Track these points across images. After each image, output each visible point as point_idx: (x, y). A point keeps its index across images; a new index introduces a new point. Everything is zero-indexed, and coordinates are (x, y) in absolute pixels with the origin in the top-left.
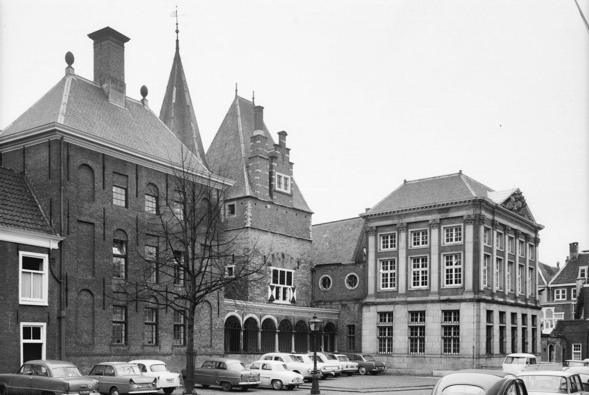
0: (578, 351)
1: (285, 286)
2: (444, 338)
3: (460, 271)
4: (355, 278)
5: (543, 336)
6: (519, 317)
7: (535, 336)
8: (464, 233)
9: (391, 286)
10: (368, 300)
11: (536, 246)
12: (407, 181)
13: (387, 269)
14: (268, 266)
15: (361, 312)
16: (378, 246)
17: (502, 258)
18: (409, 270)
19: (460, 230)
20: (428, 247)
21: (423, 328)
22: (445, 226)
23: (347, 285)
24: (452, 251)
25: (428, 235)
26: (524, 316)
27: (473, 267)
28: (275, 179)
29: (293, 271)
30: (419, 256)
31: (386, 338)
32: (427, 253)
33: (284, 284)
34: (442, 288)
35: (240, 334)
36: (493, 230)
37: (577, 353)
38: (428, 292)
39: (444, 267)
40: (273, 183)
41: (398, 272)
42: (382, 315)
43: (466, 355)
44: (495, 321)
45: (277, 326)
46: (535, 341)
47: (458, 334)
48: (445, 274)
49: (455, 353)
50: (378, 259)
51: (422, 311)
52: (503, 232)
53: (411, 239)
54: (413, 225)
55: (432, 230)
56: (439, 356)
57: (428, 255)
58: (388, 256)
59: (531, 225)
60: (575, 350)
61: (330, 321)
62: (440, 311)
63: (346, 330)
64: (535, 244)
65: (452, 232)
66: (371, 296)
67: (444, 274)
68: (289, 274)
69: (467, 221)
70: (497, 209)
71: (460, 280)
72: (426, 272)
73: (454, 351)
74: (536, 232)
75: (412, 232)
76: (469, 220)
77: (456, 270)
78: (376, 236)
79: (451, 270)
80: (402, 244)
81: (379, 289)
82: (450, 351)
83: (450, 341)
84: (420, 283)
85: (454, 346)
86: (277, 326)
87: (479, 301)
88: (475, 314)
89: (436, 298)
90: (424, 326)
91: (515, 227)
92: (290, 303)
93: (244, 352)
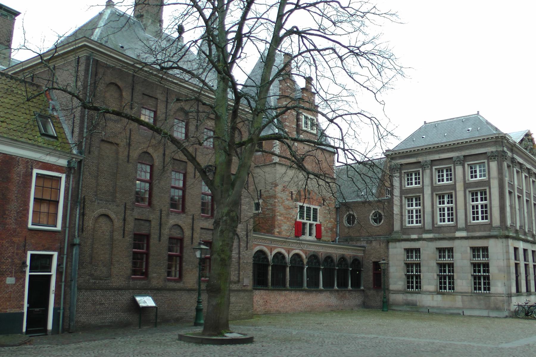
1: (312, 222)
2: (407, 275)
3: (452, 210)
6: (521, 252)
8: (455, 172)
9: (417, 223)
10: (394, 236)
13: (412, 206)
14: (295, 201)
15: (388, 249)
16: (434, 179)
18: (434, 206)
19: (451, 171)
21: (451, 265)
23: (372, 222)
24: (477, 187)
28: (302, 119)
29: (318, 208)
30: (444, 192)
32: (452, 189)
33: (310, 220)
35: (268, 269)
36: (513, 167)
38: (423, 230)
39: (436, 206)
40: (301, 123)
42: (409, 251)
43: (496, 294)
44: (530, 260)
45: (305, 261)
46: (519, 278)
47: (488, 271)
51: (450, 248)
52: (520, 171)
53: (435, 176)
54: (438, 162)
55: (456, 167)
56: (470, 294)
57: (453, 192)
58: (414, 193)
61: (356, 257)
62: (469, 249)
63: (371, 266)
66: (397, 232)
68: (315, 210)
69: (491, 157)
75: (436, 169)
76: (493, 156)
79: (477, 206)
80: (427, 181)
83: (445, 279)
84: (480, 218)
86: (305, 261)
87: (507, 237)
88: (505, 251)
89: (464, 234)
90: (453, 263)
91: (529, 166)
92: (315, 239)
93: (272, 288)
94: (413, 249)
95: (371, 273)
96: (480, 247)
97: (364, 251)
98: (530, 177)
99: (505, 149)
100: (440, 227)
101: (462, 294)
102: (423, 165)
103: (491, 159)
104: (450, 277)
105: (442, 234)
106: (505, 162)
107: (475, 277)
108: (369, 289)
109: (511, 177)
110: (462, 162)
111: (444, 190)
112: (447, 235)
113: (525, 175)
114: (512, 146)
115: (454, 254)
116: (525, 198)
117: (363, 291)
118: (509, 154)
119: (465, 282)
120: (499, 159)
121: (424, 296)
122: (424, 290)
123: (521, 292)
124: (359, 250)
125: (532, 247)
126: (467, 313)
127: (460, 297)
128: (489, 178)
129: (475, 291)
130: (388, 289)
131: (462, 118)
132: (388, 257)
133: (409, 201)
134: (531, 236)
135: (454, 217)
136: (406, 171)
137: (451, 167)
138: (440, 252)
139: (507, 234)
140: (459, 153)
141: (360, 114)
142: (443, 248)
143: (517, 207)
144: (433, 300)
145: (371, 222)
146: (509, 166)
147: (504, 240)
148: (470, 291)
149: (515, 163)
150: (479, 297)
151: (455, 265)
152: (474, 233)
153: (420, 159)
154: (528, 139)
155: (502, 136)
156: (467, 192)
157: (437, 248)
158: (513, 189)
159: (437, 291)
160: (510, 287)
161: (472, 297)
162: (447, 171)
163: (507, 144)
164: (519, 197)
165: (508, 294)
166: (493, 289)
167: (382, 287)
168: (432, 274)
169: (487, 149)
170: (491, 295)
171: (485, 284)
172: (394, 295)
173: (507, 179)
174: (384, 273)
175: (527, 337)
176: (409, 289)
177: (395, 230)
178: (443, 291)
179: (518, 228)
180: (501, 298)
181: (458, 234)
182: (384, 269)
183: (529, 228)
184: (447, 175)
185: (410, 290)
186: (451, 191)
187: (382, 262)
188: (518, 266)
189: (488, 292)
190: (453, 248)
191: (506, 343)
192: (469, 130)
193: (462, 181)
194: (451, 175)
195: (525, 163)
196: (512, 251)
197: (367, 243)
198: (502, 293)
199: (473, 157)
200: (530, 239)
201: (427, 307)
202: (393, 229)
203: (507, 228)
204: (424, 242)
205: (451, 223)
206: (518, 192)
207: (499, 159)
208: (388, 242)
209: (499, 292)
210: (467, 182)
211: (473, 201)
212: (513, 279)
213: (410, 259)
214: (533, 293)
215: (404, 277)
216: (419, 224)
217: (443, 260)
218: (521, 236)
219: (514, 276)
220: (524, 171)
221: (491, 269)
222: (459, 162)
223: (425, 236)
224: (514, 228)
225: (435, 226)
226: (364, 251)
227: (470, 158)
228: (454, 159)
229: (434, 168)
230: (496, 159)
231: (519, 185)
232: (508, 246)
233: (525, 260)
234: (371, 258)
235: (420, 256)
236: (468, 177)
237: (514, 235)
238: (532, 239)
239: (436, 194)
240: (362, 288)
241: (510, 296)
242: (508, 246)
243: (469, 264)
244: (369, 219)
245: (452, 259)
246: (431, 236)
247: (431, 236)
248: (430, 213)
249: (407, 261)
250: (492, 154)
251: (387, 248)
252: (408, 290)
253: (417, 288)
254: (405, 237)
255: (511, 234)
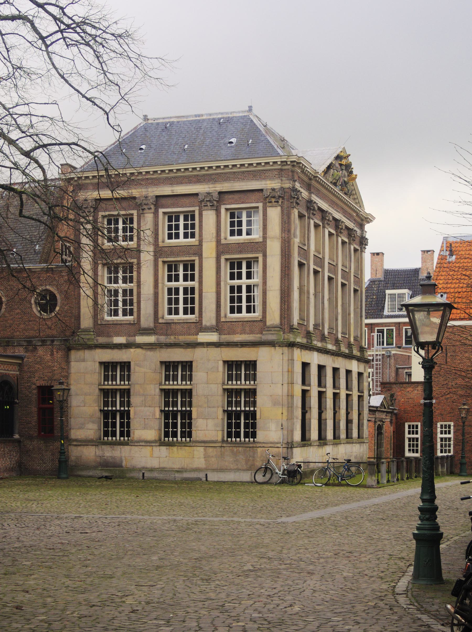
0: (447, 436)
4: (53, 297)
5: (373, 410)
6: (314, 371)
7: (307, 405)
11: (362, 251)
12: (148, 117)
17: (319, 269)
20: (197, 243)
21: (188, 393)
22: (228, 206)
24: (240, 252)
25: (197, 222)
26: (336, 370)
27: (281, 284)
30: (179, 259)
31: (116, 411)
32: (194, 254)
34: (223, 319)
36: (309, 218)
37: (446, 439)
39: (163, 283)
41: (139, 286)
44: (312, 383)
46: (307, 416)
47: (254, 404)
48: (166, 297)
49: (247, 440)
50: (160, 260)
51: (187, 362)
52: (321, 224)
54: (170, 201)
55: (204, 213)
56: (220, 445)
59: (357, 215)
60: (409, 433)
62: (221, 363)
64: (361, 248)
65: (118, 224)
66: (86, 331)
67: (226, 295)
70: (316, 180)
71: (131, 310)
72: (193, 289)
73: (246, 436)
74: (362, 227)
75: (164, 213)
77: (186, 290)
78: (156, 214)
81: (103, 319)
82: (238, 435)
83: (175, 417)
85: (122, 425)
87: (292, 345)
88: (286, 369)
89: (213, 337)
90: (191, 390)
91: (338, 216)
94: (117, 363)
95: (34, 409)
96: (241, 361)
97: (20, 365)
98: (337, 235)
99: (297, 185)
100: (168, 324)
101: (205, 443)
102: (141, 204)
103: (271, 202)
104: (185, 414)
105: (172, 337)
106: (295, 210)
107: (229, 415)
108: (31, 438)
109: (304, 236)
110: (215, 202)
111: (178, 255)
112: (182, 339)
113: (329, 232)
114: (310, 179)
115: (193, 373)
116: (327, 274)
117: (19, 441)
118: (305, 194)
119: (211, 423)
120: (286, 203)
121: (136, 449)
122: (135, 439)
123: (309, 440)
124: (11, 364)
125: (334, 361)
126: (213, 477)
127: (202, 449)
128: (265, 238)
129: (229, 439)
130: (67, 438)
131: (220, 116)
132: (67, 377)
133: (110, 272)
134: (334, 342)
135: (197, 306)
136: (107, 213)
137: (194, 211)
138: (167, 369)
139: (292, 340)
140: (211, 186)
141: (77, 145)
142: (174, 362)
143: (312, 291)
144: (152, 456)
145: (35, 310)
146: (301, 216)
147: (286, 349)
148: (220, 439)
149: (314, 210)
150: (235, 449)
151: (194, 393)
152: (232, 336)
153: (135, 192)
154: (341, 165)
155: (295, 161)
156: (223, 261)
157: (162, 363)
158: (307, 259)
159: (160, 440)
160: (291, 432)
161: (223, 448)
162: (186, 219)
163: (302, 176)
164: (316, 272)
165: (288, 443)
166: (261, 436)
167: (57, 433)
168: (152, 409)
169: (263, 182)
170: (258, 445)
171: (246, 425)
172: (79, 448)
173: (296, 241)
174: (62, 408)
175: (318, 508)
176: (108, 436)
177: (82, 327)
178: (171, 439)
179: (311, 328)
180: (274, 451)
181: (203, 337)
182: (60, 401)
183: (330, 328)
184: (186, 227)
185: (110, 438)
186: (193, 258)
187: (59, 387)
188: (307, 395)
189: (252, 440)
190: (191, 362)
191: (287, 516)
192: (231, 143)
193: (214, 240)
194: (193, 226)
195: (331, 210)
196: (298, 369)
197: (27, 350)
198: (276, 441)
199: (236, 196)
200: (330, 347)
201: (140, 470)
202: (79, 324)
203: (292, 329)
204: (139, 350)
205: (189, 316)
206: (315, 264)
207: (286, 203)
208: (69, 349)
209: (271, 440)
210: (223, 241)
211: (232, 278)
212: (297, 418)
213: (110, 383)
214: (330, 441)
215: (98, 414)
216: (128, 318)
217: (173, 385)
218: (315, 342)
219: (298, 413)
220: (329, 225)
221: (259, 399)
222: (209, 204)
223: (140, 339)
224: (304, 328)
225: (160, 321)
226: (20, 365)
227: (231, 196)
228: (200, 197)
229: (161, 211)
230: (280, 203)
231: (317, 251)
232: (293, 360)
233: (320, 385)
234: (34, 380)
235: (129, 376)
236: (225, 233)
237: (304, 341)
238: (334, 348)
239: (164, 262)
240: (17, 436)
241: (290, 446)
242: (291, 360)
243: (220, 391)
244: (31, 304)
245: (188, 383)
246: (151, 339)
247: (151, 339)
248: (151, 296)
249: (104, 385)
250: (273, 194)
251: (68, 361)
252: (106, 438)
253: (122, 435)
254: (102, 340)
255: (299, 340)
